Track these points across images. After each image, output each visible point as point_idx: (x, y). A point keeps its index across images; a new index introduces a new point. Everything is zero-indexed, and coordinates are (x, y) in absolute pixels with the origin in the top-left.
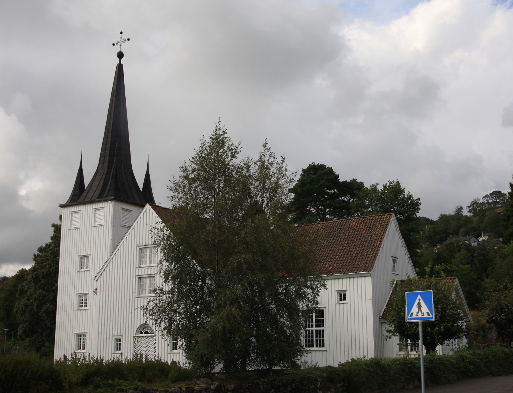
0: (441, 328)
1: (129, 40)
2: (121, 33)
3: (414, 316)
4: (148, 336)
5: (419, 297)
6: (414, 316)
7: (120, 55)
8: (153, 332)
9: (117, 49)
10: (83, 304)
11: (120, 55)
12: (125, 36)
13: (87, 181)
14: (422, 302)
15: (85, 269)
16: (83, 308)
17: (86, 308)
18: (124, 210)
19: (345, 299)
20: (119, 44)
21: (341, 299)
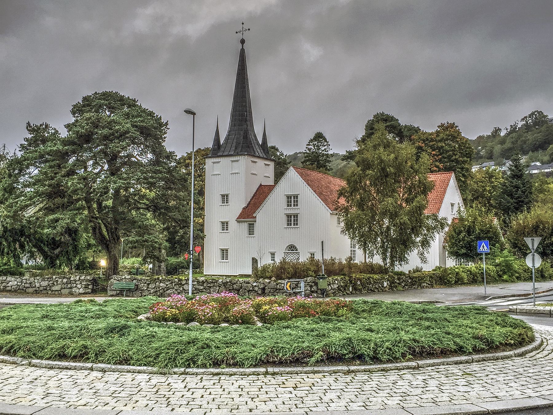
0: (84, 202)
1: (249, 30)
2: (243, 24)
3: (481, 250)
4: (294, 253)
5: (483, 243)
6: (481, 250)
7: (243, 42)
8: (297, 250)
9: (240, 36)
10: (225, 229)
11: (243, 42)
12: (246, 27)
13: (222, 141)
14: (484, 245)
15: (225, 204)
16: (225, 231)
17: (227, 231)
18: (253, 162)
19: (297, 205)
20: (242, 32)
21: (288, 206)
